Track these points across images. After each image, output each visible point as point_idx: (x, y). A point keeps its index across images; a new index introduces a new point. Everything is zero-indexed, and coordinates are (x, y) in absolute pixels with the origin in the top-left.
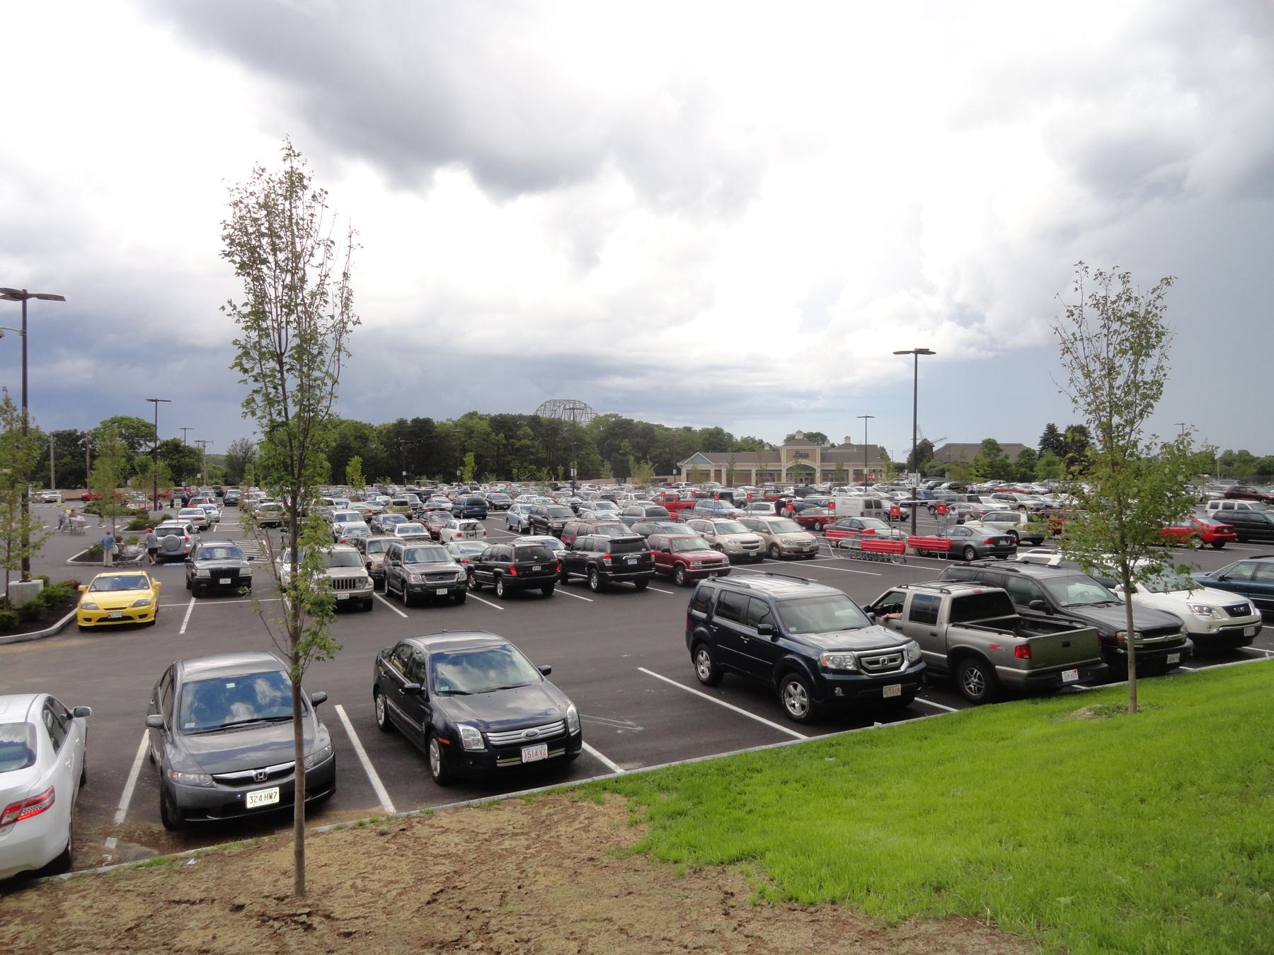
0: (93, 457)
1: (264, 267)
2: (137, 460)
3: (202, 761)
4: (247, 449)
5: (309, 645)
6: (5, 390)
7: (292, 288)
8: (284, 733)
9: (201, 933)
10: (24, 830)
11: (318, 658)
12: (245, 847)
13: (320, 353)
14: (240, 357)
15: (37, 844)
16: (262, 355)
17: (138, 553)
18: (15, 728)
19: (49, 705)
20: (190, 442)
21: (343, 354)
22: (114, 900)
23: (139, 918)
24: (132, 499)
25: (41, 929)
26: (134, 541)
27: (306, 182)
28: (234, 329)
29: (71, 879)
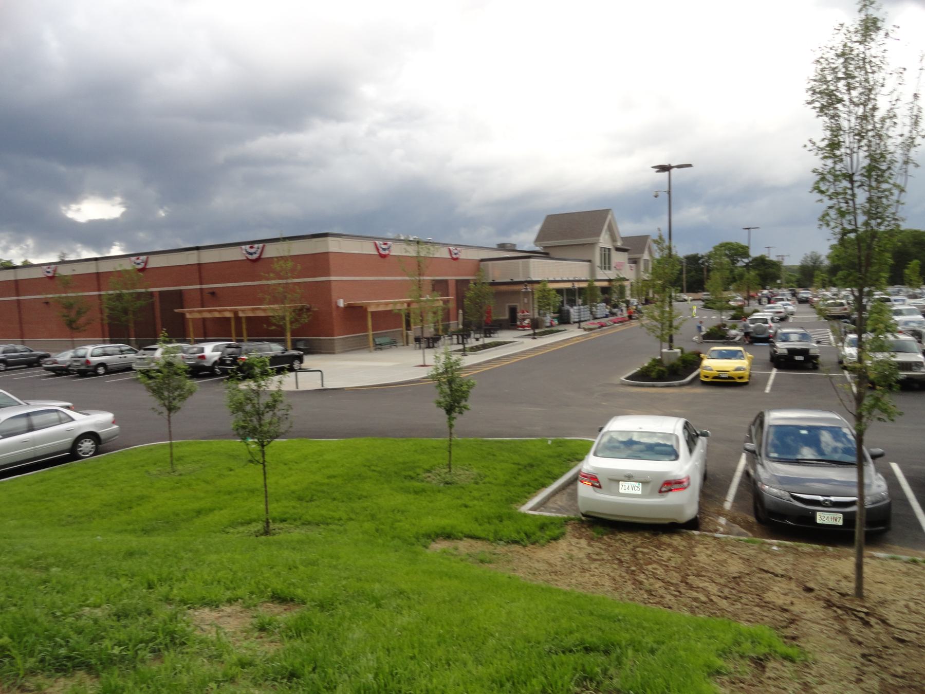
0: (709, 271)
1: (839, 106)
2: (736, 272)
3: (783, 481)
4: (816, 259)
5: (873, 407)
6: (659, 230)
7: (864, 118)
8: (849, 475)
9: (782, 597)
10: (673, 498)
11: (879, 419)
12: (814, 549)
13: (889, 168)
14: (817, 182)
15: (680, 508)
16: (836, 176)
17: (737, 335)
18: (668, 436)
19: (686, 426)
20: (773, 257)
21: (911, 167)
22: (725, 556)
23: (741, 572)
24: (733, 298)
25: (683, 559)
26: (734, 327)
27: (879, 24)
28: (817, 162)
29: (699, 535)
